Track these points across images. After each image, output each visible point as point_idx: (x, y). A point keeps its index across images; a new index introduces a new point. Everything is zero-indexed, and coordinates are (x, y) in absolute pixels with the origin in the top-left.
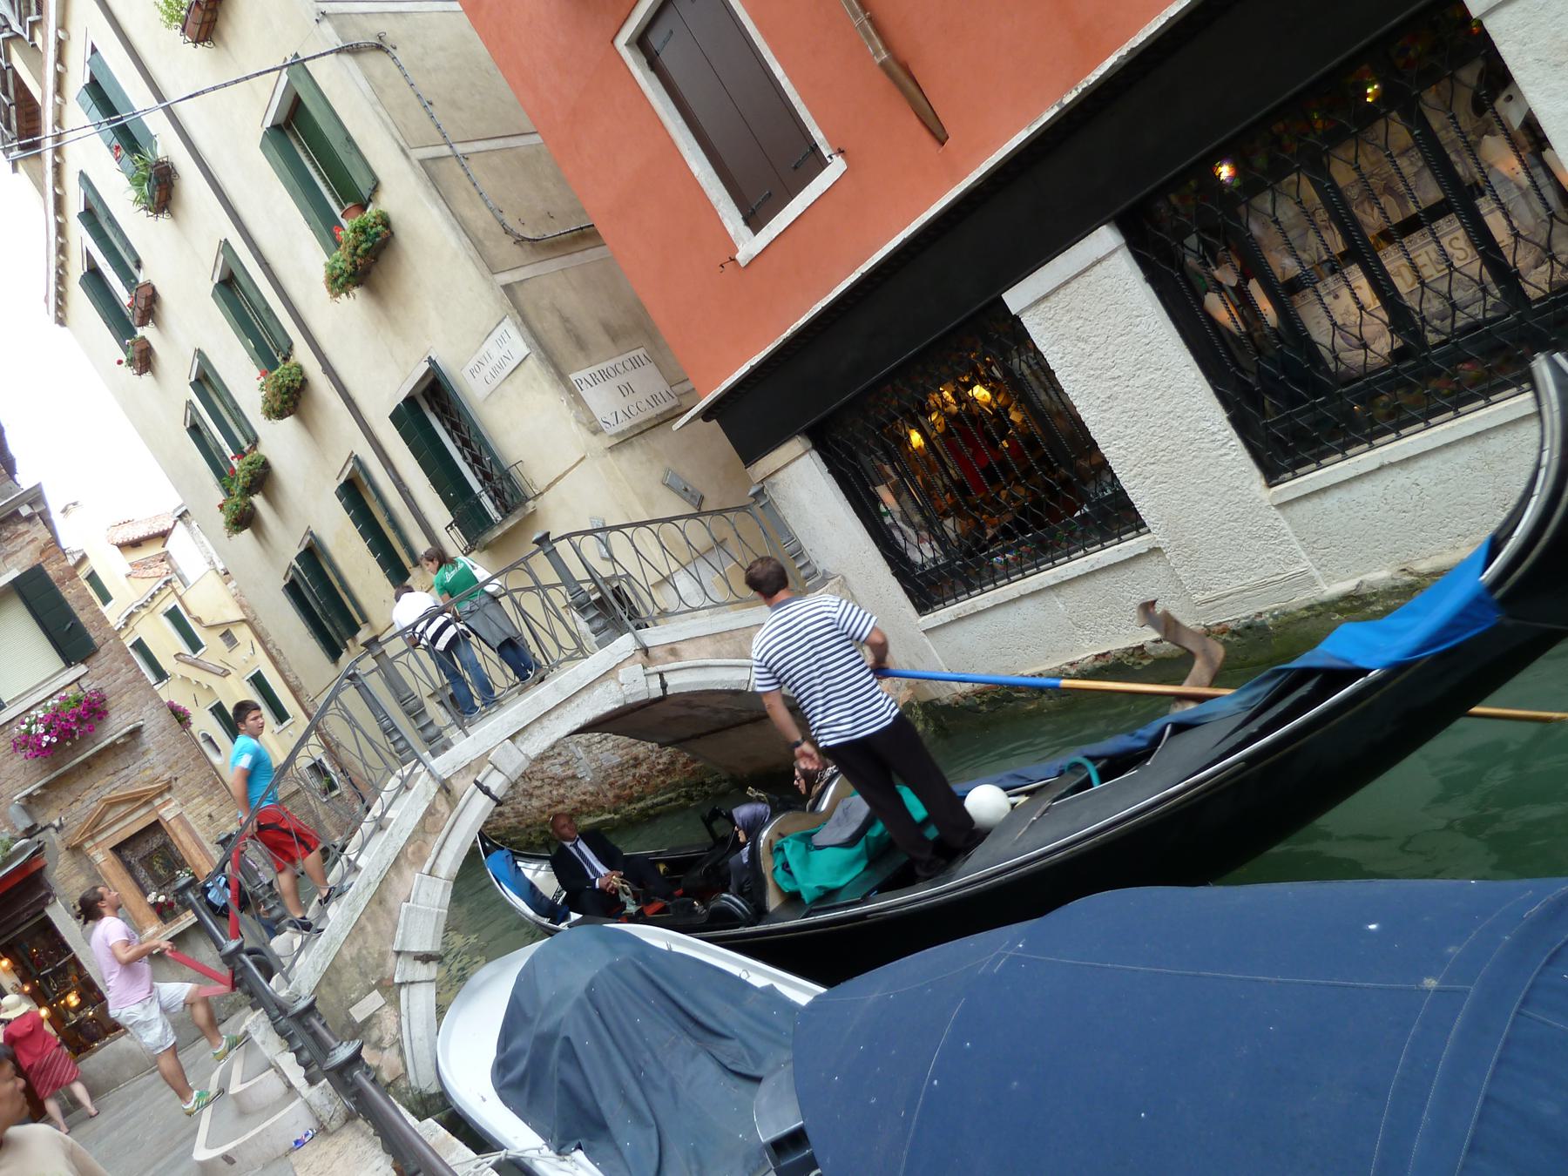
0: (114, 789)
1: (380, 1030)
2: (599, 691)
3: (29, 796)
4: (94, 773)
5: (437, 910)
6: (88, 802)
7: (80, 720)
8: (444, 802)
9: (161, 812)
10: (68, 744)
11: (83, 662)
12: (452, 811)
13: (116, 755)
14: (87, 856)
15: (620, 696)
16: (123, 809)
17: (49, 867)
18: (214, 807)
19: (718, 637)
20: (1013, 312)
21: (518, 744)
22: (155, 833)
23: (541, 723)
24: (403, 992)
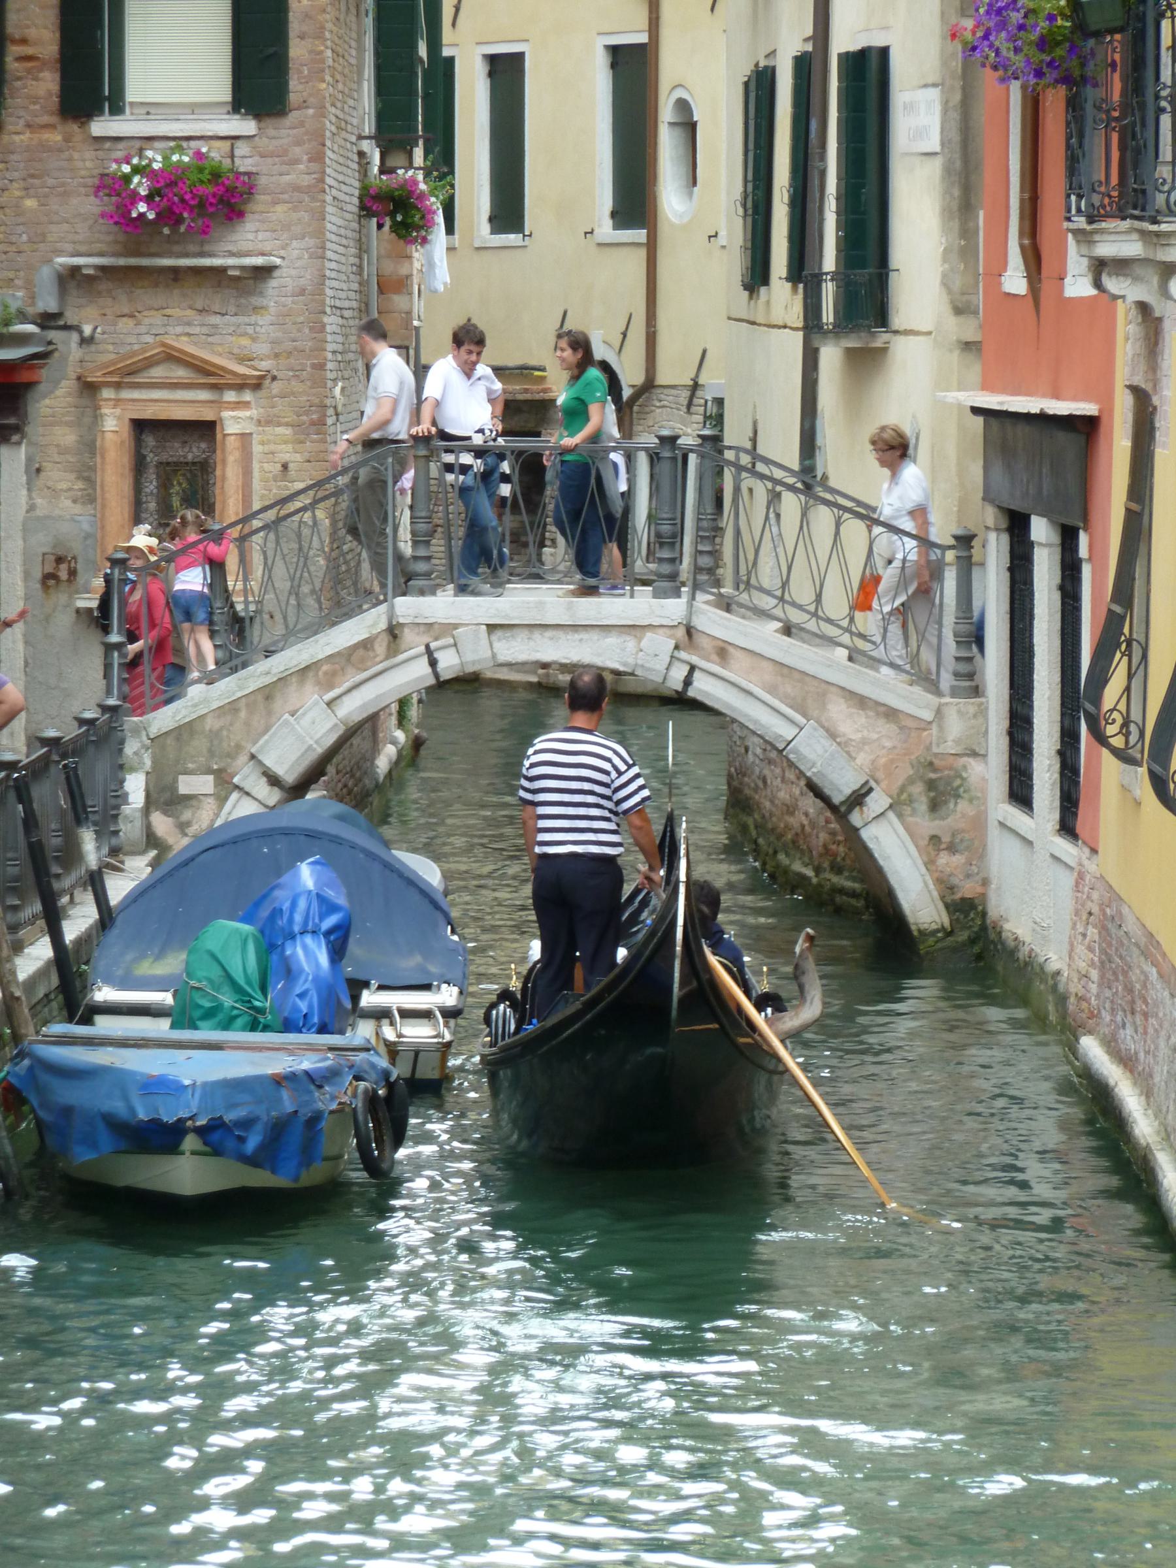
0: (188, 334)
1: (193, 815)
2: (612, 640)
3: (75, 270)
4: (176, 291)
5: (311, 742)
6: (143, 329)
7: (202, 206)
8: (385, 644)
9: (226, 414)
10: (166, 231)
11: (258, 116)
12: (387, 658)
13: (219, 286)
14: (97, 408)
15: (631, 661)
16: (181, 373)
17: (42, 387)
18: (298, 457)
19: (785, 671)
20: (1033, 538)
21: (494, 638)
22: (202, 438)
23: (531, 632)
24: (235, 796)
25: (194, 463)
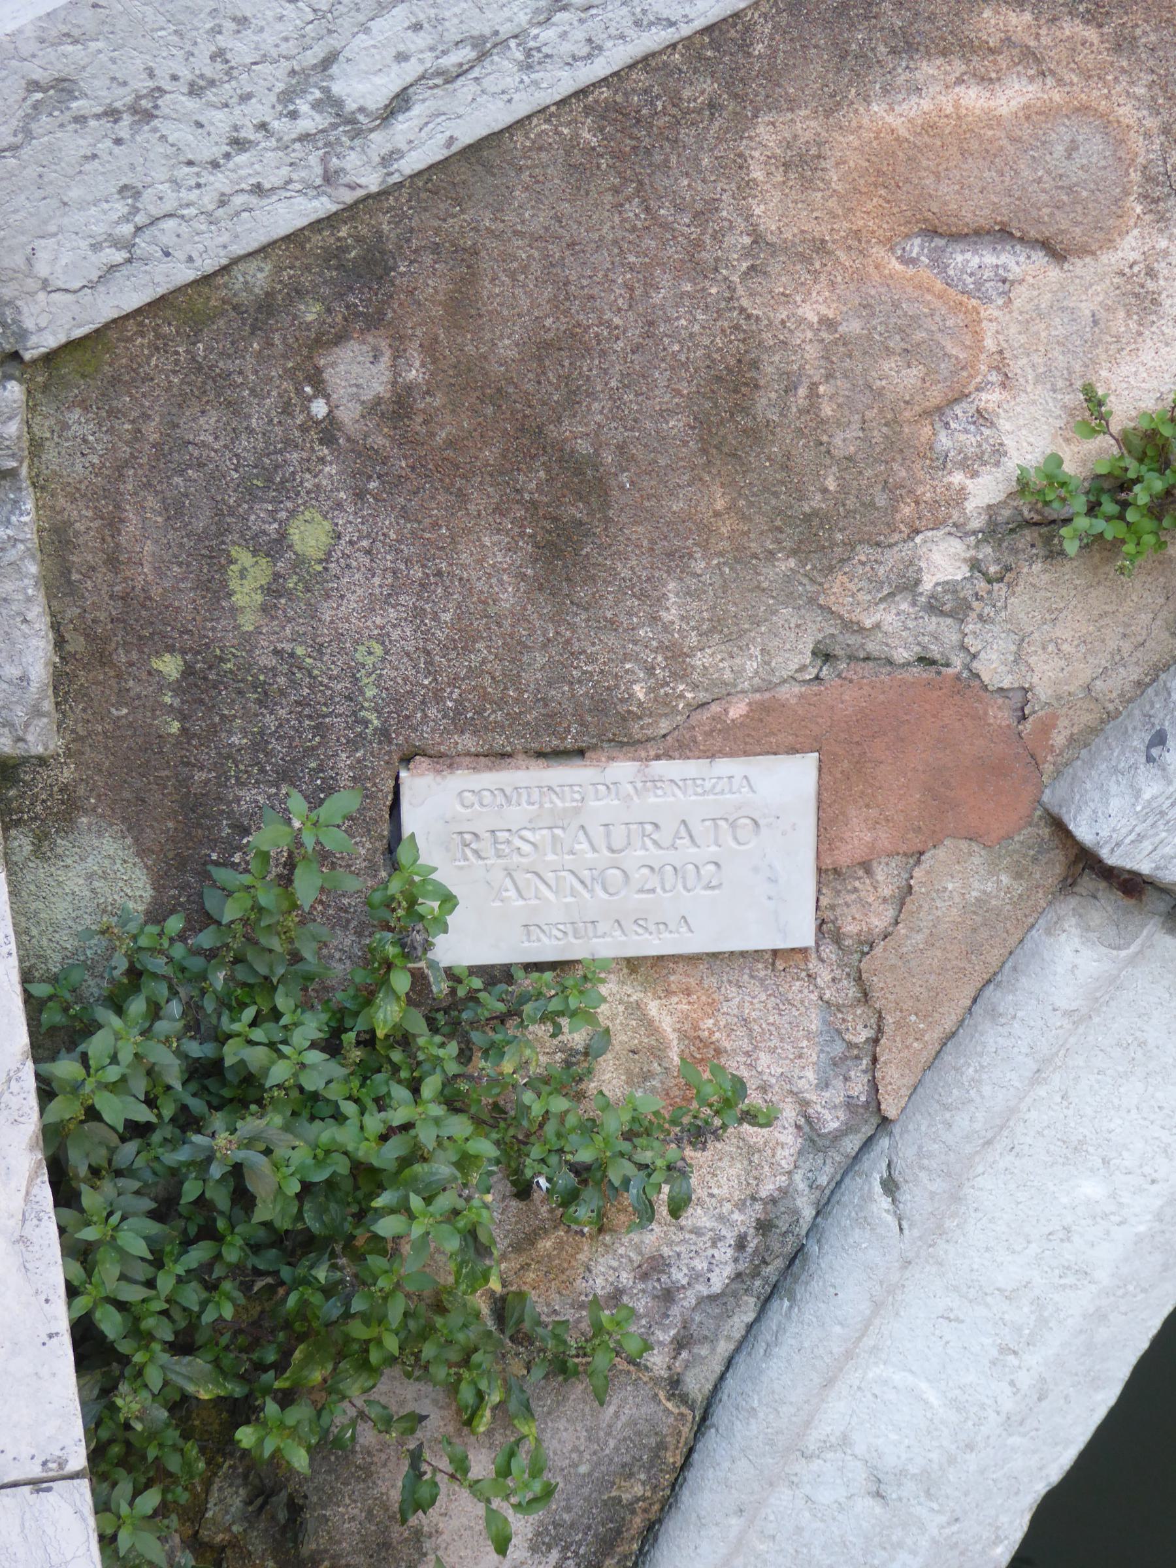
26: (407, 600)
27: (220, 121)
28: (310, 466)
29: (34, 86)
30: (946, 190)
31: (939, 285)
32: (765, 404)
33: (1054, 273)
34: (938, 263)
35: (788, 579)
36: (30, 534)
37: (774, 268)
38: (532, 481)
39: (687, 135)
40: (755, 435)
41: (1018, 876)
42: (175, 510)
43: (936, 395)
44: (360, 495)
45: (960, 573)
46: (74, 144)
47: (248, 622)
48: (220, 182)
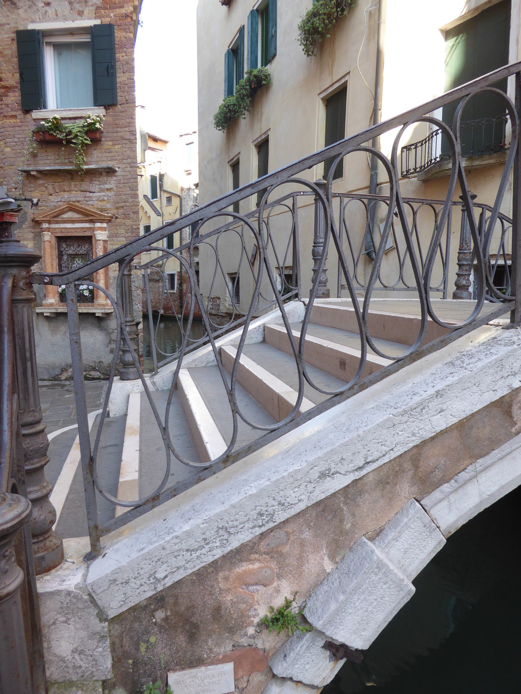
16: (75, 216)
25: (83, 254)
26: (168, 647)
27: (138, 582)
28: (153, 629)
29: (111, 580)
30: (248, 580)
31: (248, 592)
32: (223, 612)
33: (264, 588)
34: (247, 588)
35: (228, 636)
36: (109, 645)
37: (223, 592)
38: (187, 627)
39: (209, 576)
40: (221, 617)
41: (266, 676)
42: (131, 638)
43: (248, 608)
44: (160, 632)
45: (253, 632)
46: (116, 588)
47: (143, 654)
48: (138, 591)
